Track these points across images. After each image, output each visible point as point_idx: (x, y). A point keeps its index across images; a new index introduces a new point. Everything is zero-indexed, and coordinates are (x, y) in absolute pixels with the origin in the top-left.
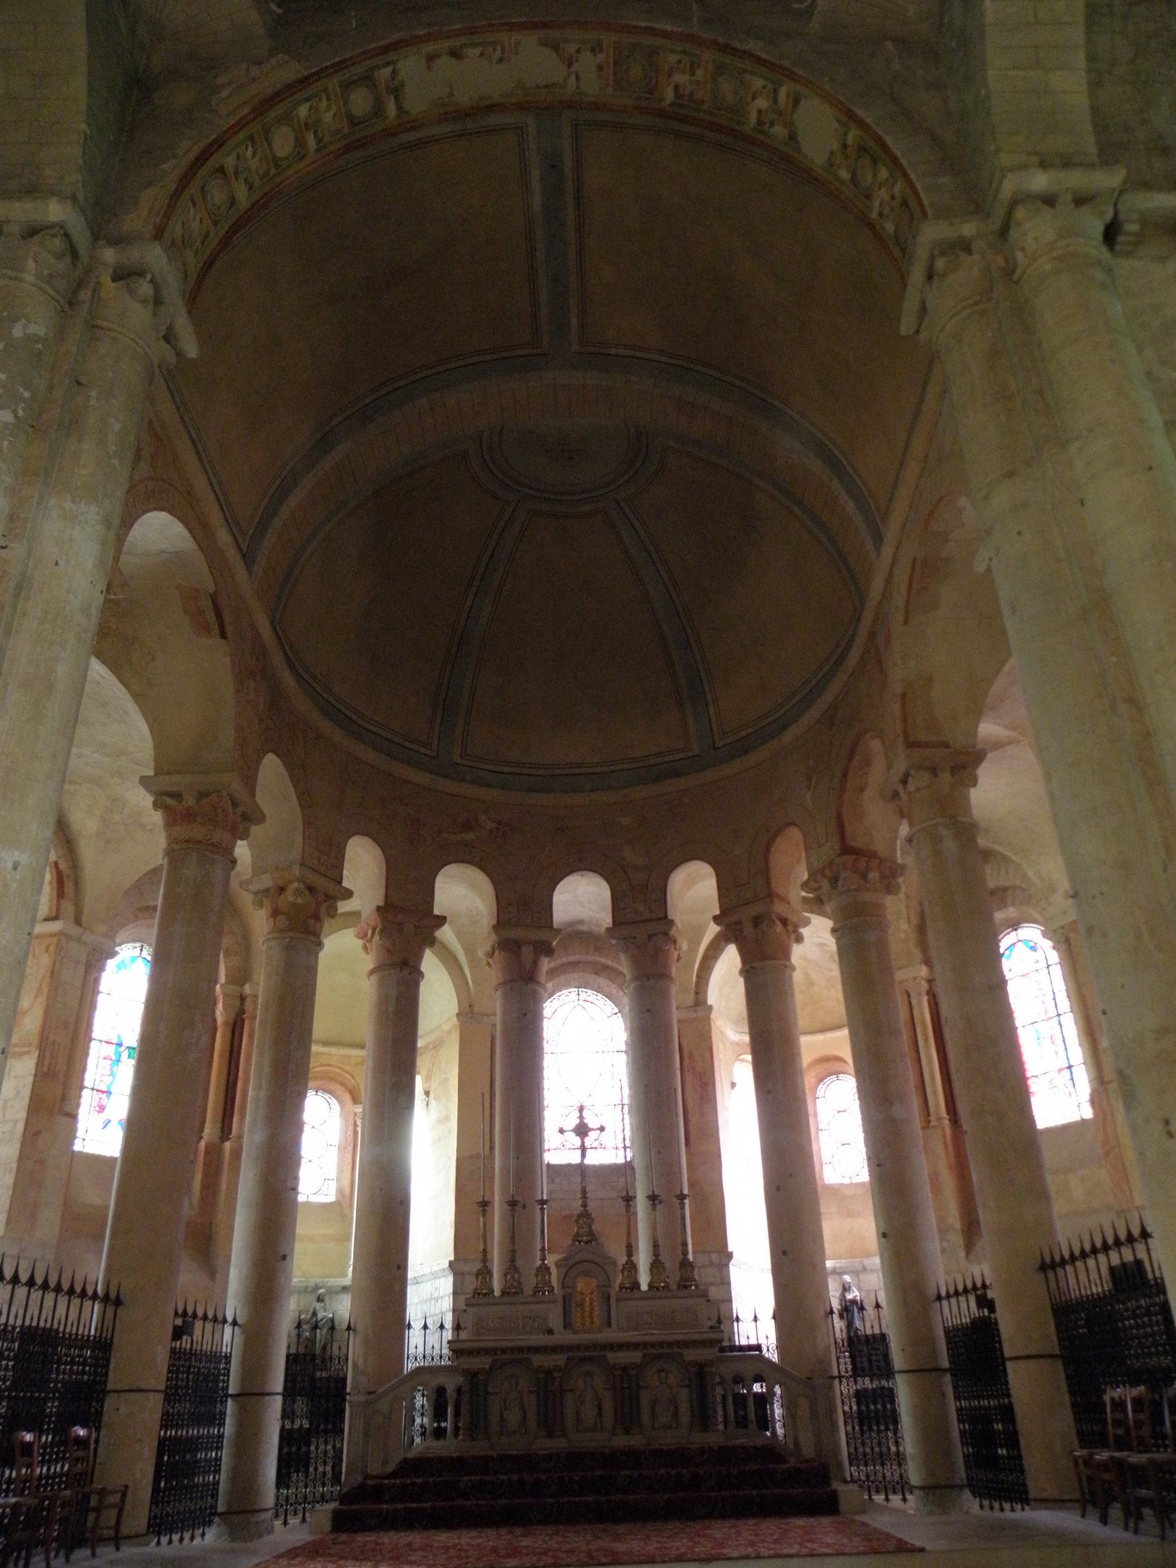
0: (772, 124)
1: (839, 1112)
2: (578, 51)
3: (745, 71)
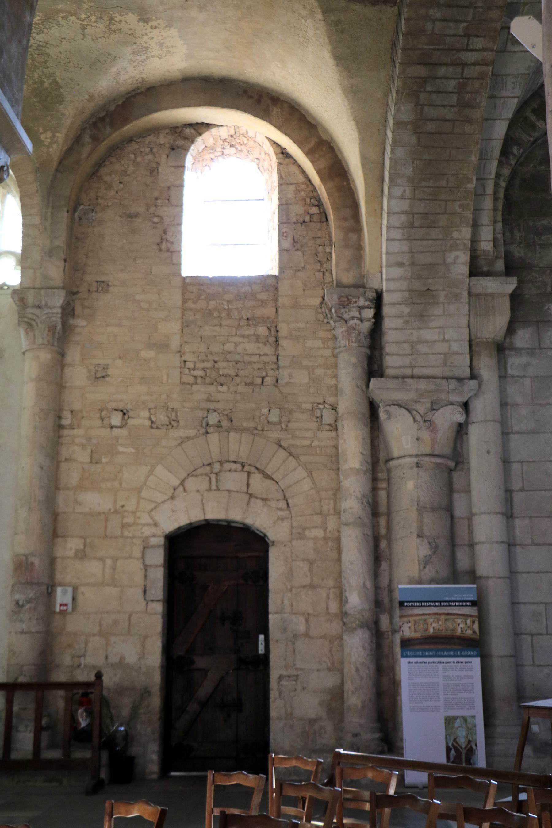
0: (466, 631)
1: (263, 200)
2: (403, 624)
3: (455, 619)
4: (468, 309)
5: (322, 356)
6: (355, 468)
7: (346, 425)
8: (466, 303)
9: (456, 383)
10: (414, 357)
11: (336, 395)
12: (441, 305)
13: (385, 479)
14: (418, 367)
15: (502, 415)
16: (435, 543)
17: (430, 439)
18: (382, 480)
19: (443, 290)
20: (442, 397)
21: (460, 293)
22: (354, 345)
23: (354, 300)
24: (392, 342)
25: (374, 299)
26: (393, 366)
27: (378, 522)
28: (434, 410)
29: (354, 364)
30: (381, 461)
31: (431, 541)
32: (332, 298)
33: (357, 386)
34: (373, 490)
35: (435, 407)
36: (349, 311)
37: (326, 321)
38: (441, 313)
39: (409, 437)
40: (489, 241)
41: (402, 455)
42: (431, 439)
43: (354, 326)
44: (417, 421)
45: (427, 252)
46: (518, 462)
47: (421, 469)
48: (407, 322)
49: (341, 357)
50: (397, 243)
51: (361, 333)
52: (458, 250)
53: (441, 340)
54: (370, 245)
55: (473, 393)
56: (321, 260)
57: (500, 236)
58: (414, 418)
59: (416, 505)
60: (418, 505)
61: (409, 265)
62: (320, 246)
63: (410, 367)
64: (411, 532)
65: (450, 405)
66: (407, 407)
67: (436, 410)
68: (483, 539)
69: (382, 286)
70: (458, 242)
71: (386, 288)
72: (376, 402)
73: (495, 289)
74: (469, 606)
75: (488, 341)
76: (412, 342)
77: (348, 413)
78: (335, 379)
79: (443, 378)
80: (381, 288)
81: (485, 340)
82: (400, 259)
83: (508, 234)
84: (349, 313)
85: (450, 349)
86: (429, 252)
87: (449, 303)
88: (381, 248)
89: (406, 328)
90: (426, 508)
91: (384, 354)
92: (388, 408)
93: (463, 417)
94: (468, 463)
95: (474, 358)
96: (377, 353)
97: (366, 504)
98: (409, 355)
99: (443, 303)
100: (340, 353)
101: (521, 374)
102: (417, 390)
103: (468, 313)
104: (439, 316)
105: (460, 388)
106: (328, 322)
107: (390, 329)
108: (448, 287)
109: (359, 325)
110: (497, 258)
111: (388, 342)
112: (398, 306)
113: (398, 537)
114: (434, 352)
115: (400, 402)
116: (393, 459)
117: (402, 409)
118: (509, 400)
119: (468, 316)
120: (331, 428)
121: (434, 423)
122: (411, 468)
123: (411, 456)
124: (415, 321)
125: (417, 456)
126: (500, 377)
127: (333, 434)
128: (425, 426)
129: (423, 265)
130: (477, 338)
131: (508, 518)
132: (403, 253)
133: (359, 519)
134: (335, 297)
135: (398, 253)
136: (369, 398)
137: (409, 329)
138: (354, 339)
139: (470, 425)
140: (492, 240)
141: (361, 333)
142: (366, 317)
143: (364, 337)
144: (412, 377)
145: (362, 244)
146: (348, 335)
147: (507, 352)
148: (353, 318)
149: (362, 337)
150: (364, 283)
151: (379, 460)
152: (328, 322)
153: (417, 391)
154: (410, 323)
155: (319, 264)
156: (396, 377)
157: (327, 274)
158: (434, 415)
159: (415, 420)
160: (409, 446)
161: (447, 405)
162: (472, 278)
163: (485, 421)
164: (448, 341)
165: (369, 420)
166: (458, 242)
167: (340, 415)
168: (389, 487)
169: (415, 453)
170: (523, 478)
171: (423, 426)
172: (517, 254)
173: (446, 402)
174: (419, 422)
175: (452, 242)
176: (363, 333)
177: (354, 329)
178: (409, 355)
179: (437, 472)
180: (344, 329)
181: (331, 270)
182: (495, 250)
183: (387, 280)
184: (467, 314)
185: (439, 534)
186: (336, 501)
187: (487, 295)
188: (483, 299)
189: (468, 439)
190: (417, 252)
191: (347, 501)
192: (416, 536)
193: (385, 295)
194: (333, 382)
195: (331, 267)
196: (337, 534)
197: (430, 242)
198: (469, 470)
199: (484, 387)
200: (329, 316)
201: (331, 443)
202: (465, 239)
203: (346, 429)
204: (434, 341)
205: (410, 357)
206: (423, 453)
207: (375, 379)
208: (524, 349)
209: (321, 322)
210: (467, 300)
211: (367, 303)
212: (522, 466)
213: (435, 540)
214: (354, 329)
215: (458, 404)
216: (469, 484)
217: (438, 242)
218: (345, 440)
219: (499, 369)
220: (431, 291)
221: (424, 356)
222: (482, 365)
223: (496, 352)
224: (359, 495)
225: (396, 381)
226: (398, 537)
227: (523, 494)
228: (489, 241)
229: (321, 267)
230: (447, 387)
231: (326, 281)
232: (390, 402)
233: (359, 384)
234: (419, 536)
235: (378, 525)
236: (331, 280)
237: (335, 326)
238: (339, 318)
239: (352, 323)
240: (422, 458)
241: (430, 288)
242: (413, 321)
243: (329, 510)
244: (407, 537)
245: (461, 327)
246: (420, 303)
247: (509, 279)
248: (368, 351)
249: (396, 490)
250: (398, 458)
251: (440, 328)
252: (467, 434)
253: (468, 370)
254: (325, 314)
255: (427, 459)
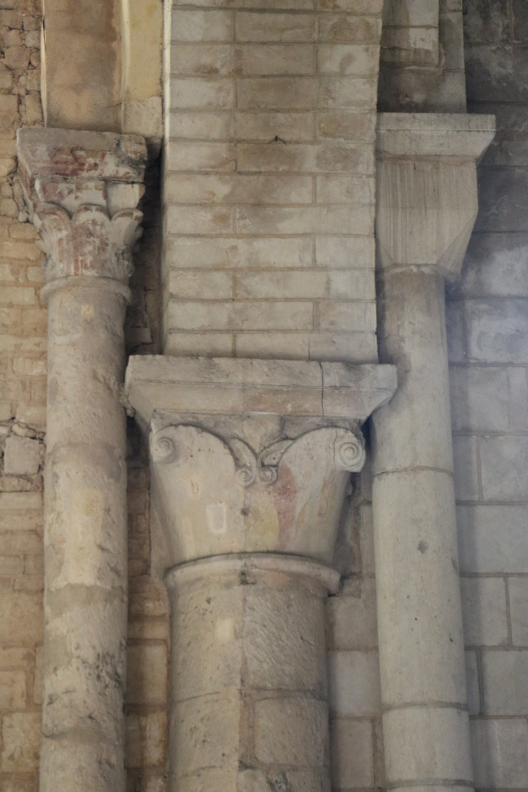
4: (373, 190)
5: (11, 305)
6: (81, 586)
7: (62, 475)
8: (369, 176)
9: (342, 372)
10: (239, 305)
11: (44, 403)
12: (309, 180)
13: (163, 616)
14: (250, 331)
15: (456, 458)
16: (286, 783)
17: (275, 512)
18: (155, 618)
19: (312, 143)
20: (307, 406)
21: (354, 151)
22: (90, 273)
23: (91, 161)
24: (183, 269)
25: (142, 161)
26: (186, 327)
27: (142, 729)
28: (287, 438)
29: (89, 323)
30: (153, 571)
31: (275, 778)
32: (33, 152)
33: (95, 377)
34: (128, 644)
35: (291, 433)
36: (78, 189)
37: (22, 217)
38: (308, 199)
39: (224, 507)
40: (428, 27)
41: (206, 551)
42: (279, 513)
43: (91, 227)
44: (245, 465)
45: (273, 43)
46: (498, 575)
47: (253, 587)
48: (222, 219)
49: (55, 303)
50: (199, 17)
51: (107, 245)
52: (352, 41)
53: (305, 265)
54: (134, 25)
55: (384, 397)
56: (13, 65)
57: (455, 18)
58: (236, 460)
59: (238, 681)
60: (242, 681)
61: (229, 75)
62: (11, 29)
63: (228, 331)
64: (223, 755)
65: (327, 427)
66: (219, 430)
67: (291, 439)
68: (409, 774)
69: (164, 129)
70: (352, 20)
71: (172, 130)
72: (142, 420)
73: (441, 144)
75: (423, 273)
76: (235, 270)
77: (70, 444)
78: (41, 363)
79: (310, 359)
80: (160, 134)
81: (415, 270)
82: (206, 59)
83: (476, 21)
84: (79, 194)
85: (328, 289)
86: (280, 43)
87: (327, 176)
88: (162, 36)
89: (220, 235)
90: (265, 689)
91: (166, 295)
92: (171, 432)
93: (358, 459)
94: (373, 576)
95: (387, 313)
96: (150, 300)
97: (107, 679)
98: (226, 301)
99: (314, 176)
100: (53, 293)
101: (503, 357)
102: (244, 388)
103: (374, 201)
104: (301, 205)
105: (351, 385)
106: (28, 221)
107: (180, 235)
108: (326, 134)
109: (102, 225)
110: (448, 70)
111: (174, 269)
112: (200, 178)
113: (192, 767)
114: (289, 294)
115: (201, 418)
116: (183, 563)
117: (205, 434)
118: (475, 422)
119: (373, 209)
120: (29, 486)
121: (288, 471)
122: (228, 586)
123: (228, 554)
124: (242, 218)
125: (242, 554)
126: (452, 365)
127: (34, 500)
128: (262, 480)
129: (264, 76)
130: (396, 265)
131: (472, 718)
132: (214, 42)
133: (89, 721)
134: (42, 150)
135: (203, 42)
136: (125, 409)
137: (228, 236)
138: (89, 259)
139: (376, 480)
140: (437, 26)
141: (107, 245)
142: (121, 206)
143: (116, 254)
144: (234, 355)
145: (114, 24)
146: (76, 248)
147: (469, 304)
148: (87, 207)
149: (110, 254)
150: (117, 122)
151: (149, 566)
152: (28, 221)
153: (244, 390)
154: (231, 221)
155: (8, 76)
156: (194, 355)
157: (28, 101)
158: (286, 450)
159: (238, 463)
160: (223, 531)
161: (319, 427)
162: (386, 115)
163: (415, 469)
164: (325, 268)
165: (122, 464)
166: (352, 20)
167: (49, 450)
168: (172, 637)
169: (237, 546)
170: (508, 616)
171: (258, 479)
172: (495, 69)
173: (317, 420)
174: (251, 470)
175: (335, 19)
176: (114, 244)
177: (91, 234)
178: (226, 301)
179: (292, 596)
180: (64, 233)
181: (39, 92)
182: (443, 51)
183: (173, 110)
184: (370, 205)
185: (296, 758)
186: (33, 673)
187: (419, 158)
188: (411, 167)
189: (371, 516)
190: (249, 43)
191: (59, 672)
192: (237, 764)
193: (168, 149)
194: (37, 369)
195: (39, 85)
196: (31, 764)
197: (282, 18)
198: (373, 593)
199: (411, 386)
200: (30, 203)
201: (26, 523)
202: (370, 14)
203: (63, 480)
204: (291, 269)
205: (228, 305)
206: (259, 549)
207: (138, 356)
208: (510, 297)
209: (10, 220)
210: (372, 170)
211: (123, 170)
212: (506, 587)
213: (284, 777)
214: (91, 234)
215: (348, 426)
216: (374, 631)
217: (304, 19)
218: (59, 515)
219: (450, 345)
220: (284, 142)
221: (265, 305)
222: (406, 331)
223: (442, 300)
224: (90, 656)
225: (192, 364)
226: (192, 767)
227: (511, 656)
228: (428, 27)
229: (14, 82)
230: (319, 380)
231: (24, 119)
232: (178, 418)
233: (101, 372)
234: (243, 766)
235: (143, 738)
236: (38, 116)
237: (43, 225)
238: (53, 206)
239: (84, 217)
240: (255, 561)
241: (281, 136)
242: (238, 216)
243: (12, 700)
244: (214, 767)
245: (357, 236)
246: (256, 173)
247: (477, 119)
248: (126, 292)
249: (188, 644)
250: (195, 560)
251: (304, 235)
252: (369, 503)
253: (372, 341)
254: (21, 200)
255: (268, 562)
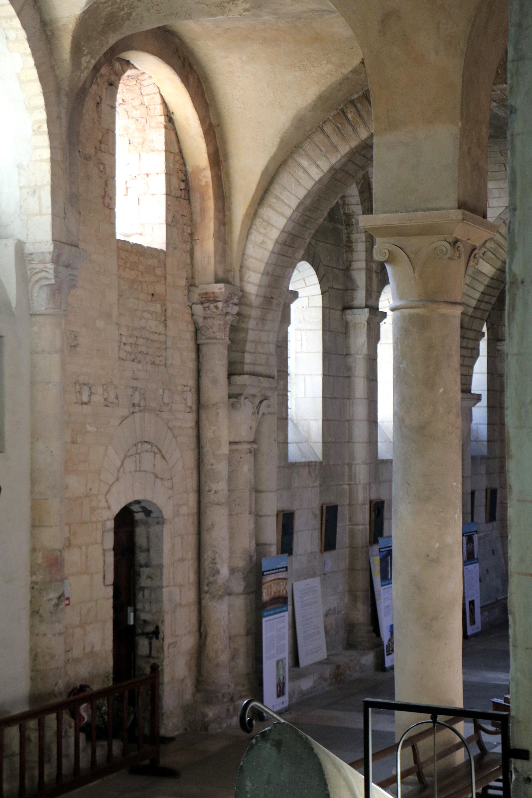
74: (284, 571)
122: (247, 453)
180: (222, 322)
